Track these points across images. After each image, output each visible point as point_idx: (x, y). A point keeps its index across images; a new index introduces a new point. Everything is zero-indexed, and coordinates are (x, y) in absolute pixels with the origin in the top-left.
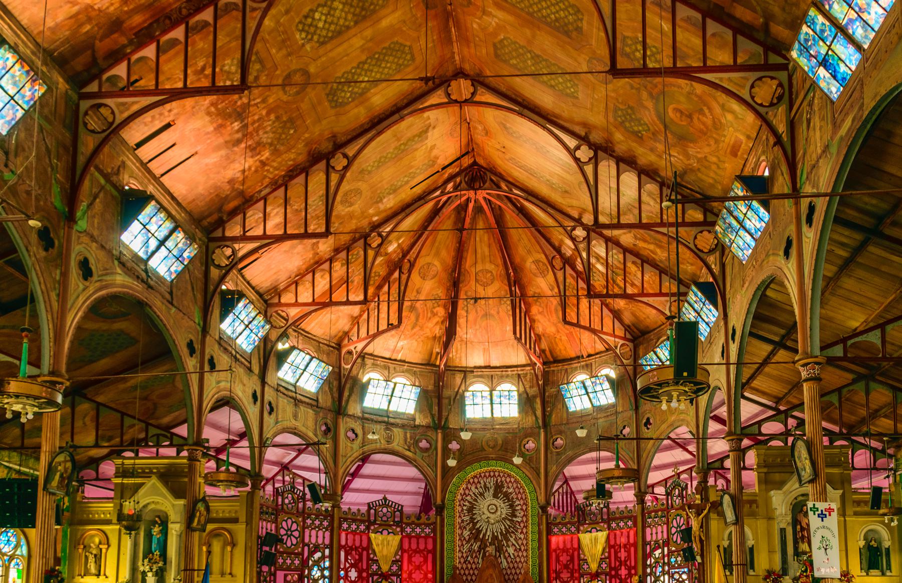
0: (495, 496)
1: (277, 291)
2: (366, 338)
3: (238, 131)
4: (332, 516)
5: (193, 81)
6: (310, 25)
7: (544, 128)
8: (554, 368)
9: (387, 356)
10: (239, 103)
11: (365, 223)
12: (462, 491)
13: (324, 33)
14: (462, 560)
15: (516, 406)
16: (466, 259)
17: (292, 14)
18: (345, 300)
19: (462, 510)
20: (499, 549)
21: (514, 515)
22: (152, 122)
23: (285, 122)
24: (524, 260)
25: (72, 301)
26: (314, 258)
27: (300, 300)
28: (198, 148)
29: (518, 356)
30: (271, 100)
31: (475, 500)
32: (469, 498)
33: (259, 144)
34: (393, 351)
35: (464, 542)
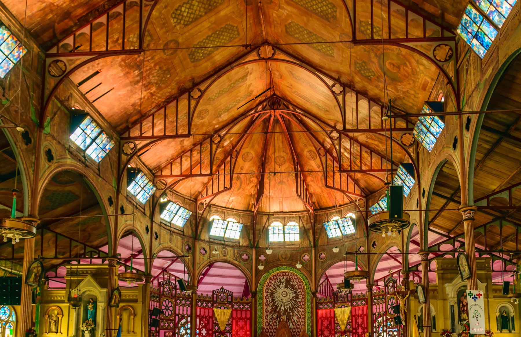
0: (286, 287)
1: (160, 168)
2: (212, 196)
3: (137, 76)
4: (192, 299)
5: (111, 47)
6: (179, 15)
7: (314, 74)
8: (320, 213)
9: (224, 206)
10: (138, 60)
11: (211, 129)
12: (267, 284)
13: (187, 19)
14: (267, 324)
15: (298, 235)
16: (269, 150)
17: (169, 8)
18: (199, 173)
19: (267, 295)
20: (288, 317)
21: (297, 298)
22: (88, 70)
23: (165, 71)
24: (302, 150)
25: (41, 174)
26: (181, 149)
27: (173, 174)
28: (114, 86)
29: (299, 206)
30: (156, 58)
31: (275, 289)
32: (271, 288)
33: (149, 83)
34: (227, 203)
35: (268, 314)
